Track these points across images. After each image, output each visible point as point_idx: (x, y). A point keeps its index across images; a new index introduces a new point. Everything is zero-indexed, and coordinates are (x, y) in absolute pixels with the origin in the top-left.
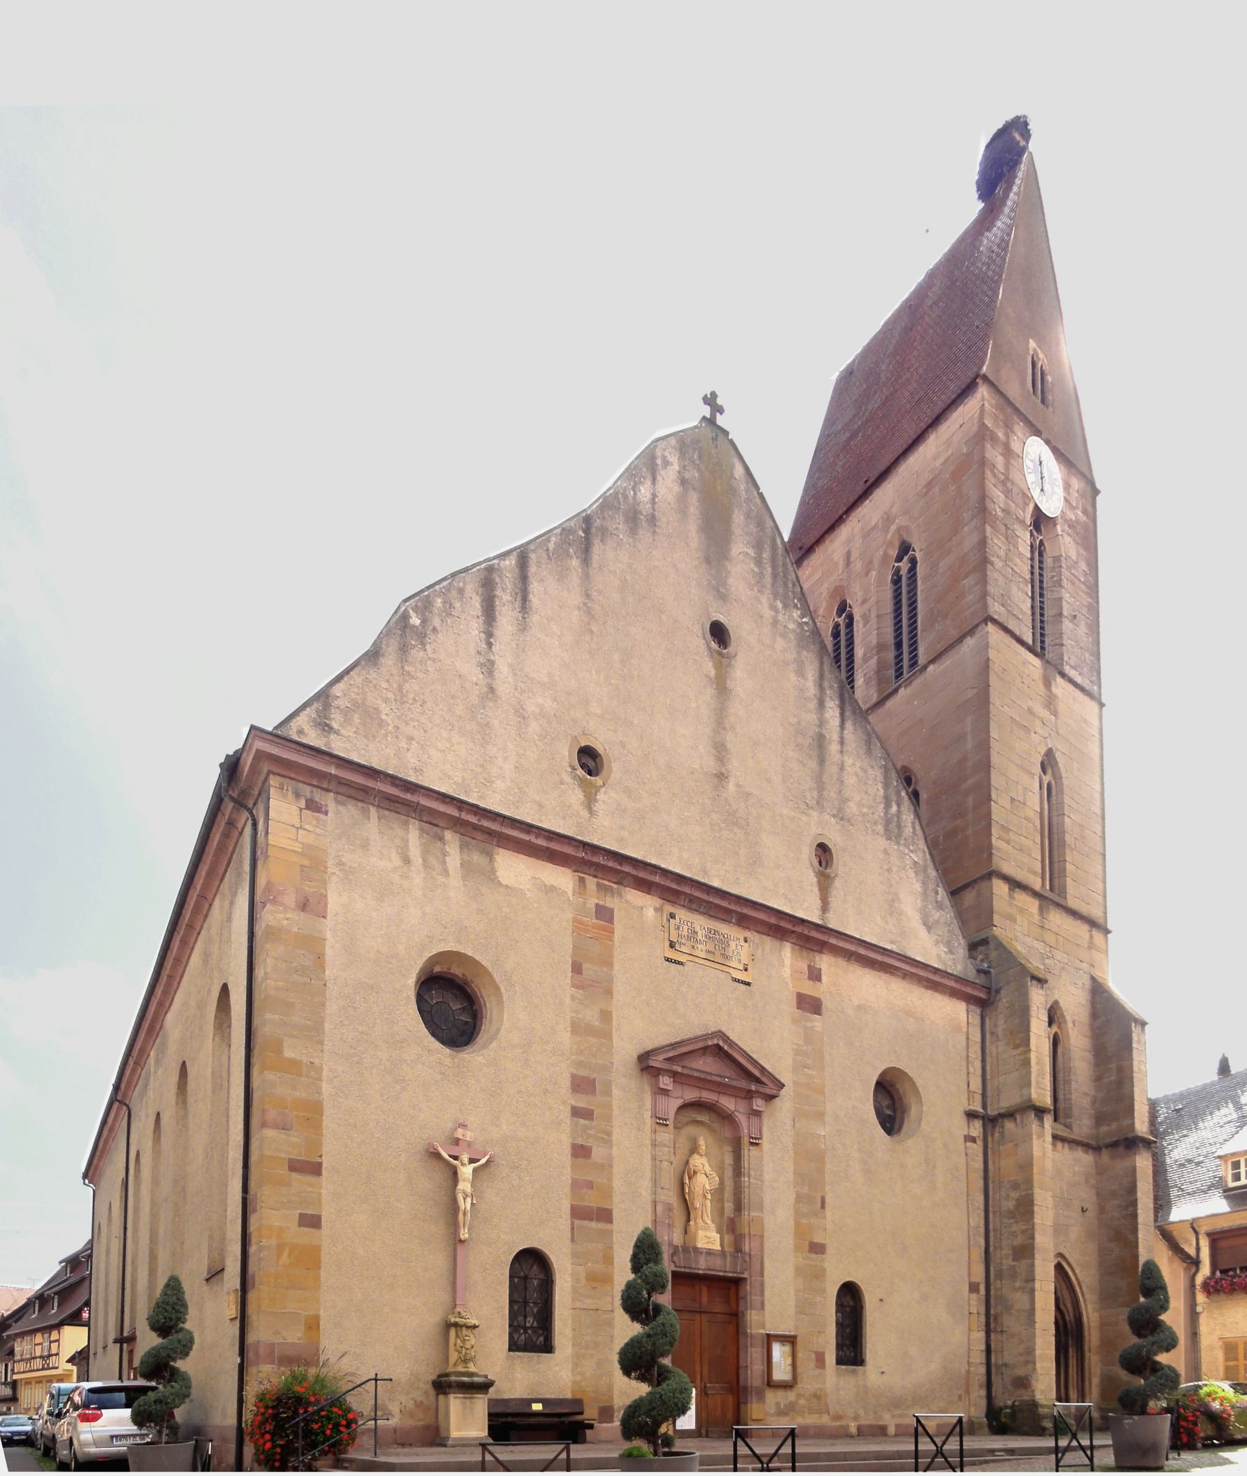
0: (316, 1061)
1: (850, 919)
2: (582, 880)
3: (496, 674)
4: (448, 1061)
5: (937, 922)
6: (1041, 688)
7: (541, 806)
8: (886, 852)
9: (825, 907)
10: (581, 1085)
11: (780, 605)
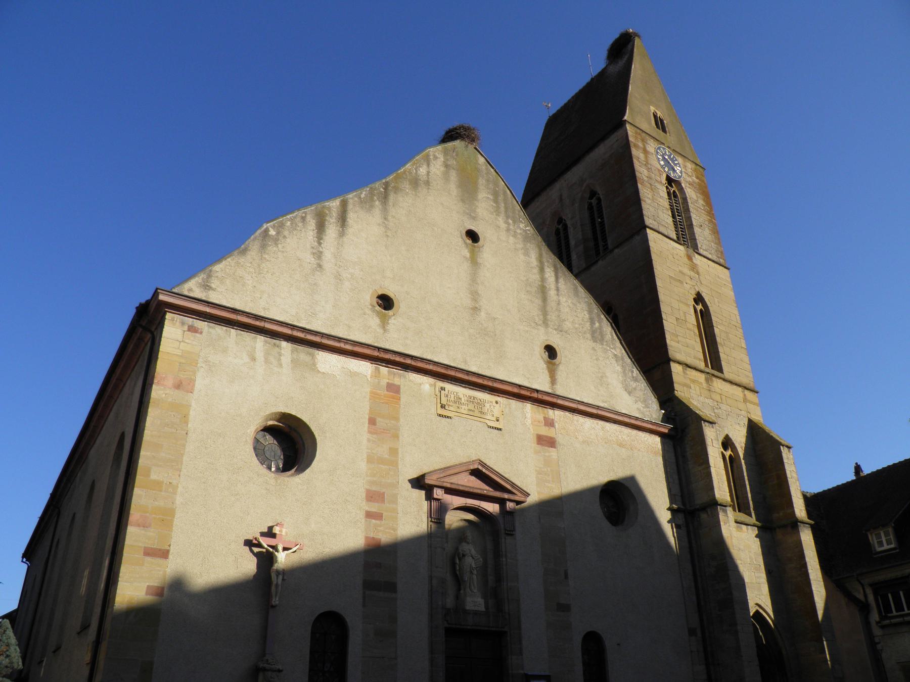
0: (174, 482)
1: (567, 388)
2: (377, 370)
3: (323, 258)
4: (272, 482)
5: (635, 389)
6: (686, 260)
7: (349, 327)
8: (593, 349)
9: (553, 381)
10: (373, 496)
11: (511, 222)
